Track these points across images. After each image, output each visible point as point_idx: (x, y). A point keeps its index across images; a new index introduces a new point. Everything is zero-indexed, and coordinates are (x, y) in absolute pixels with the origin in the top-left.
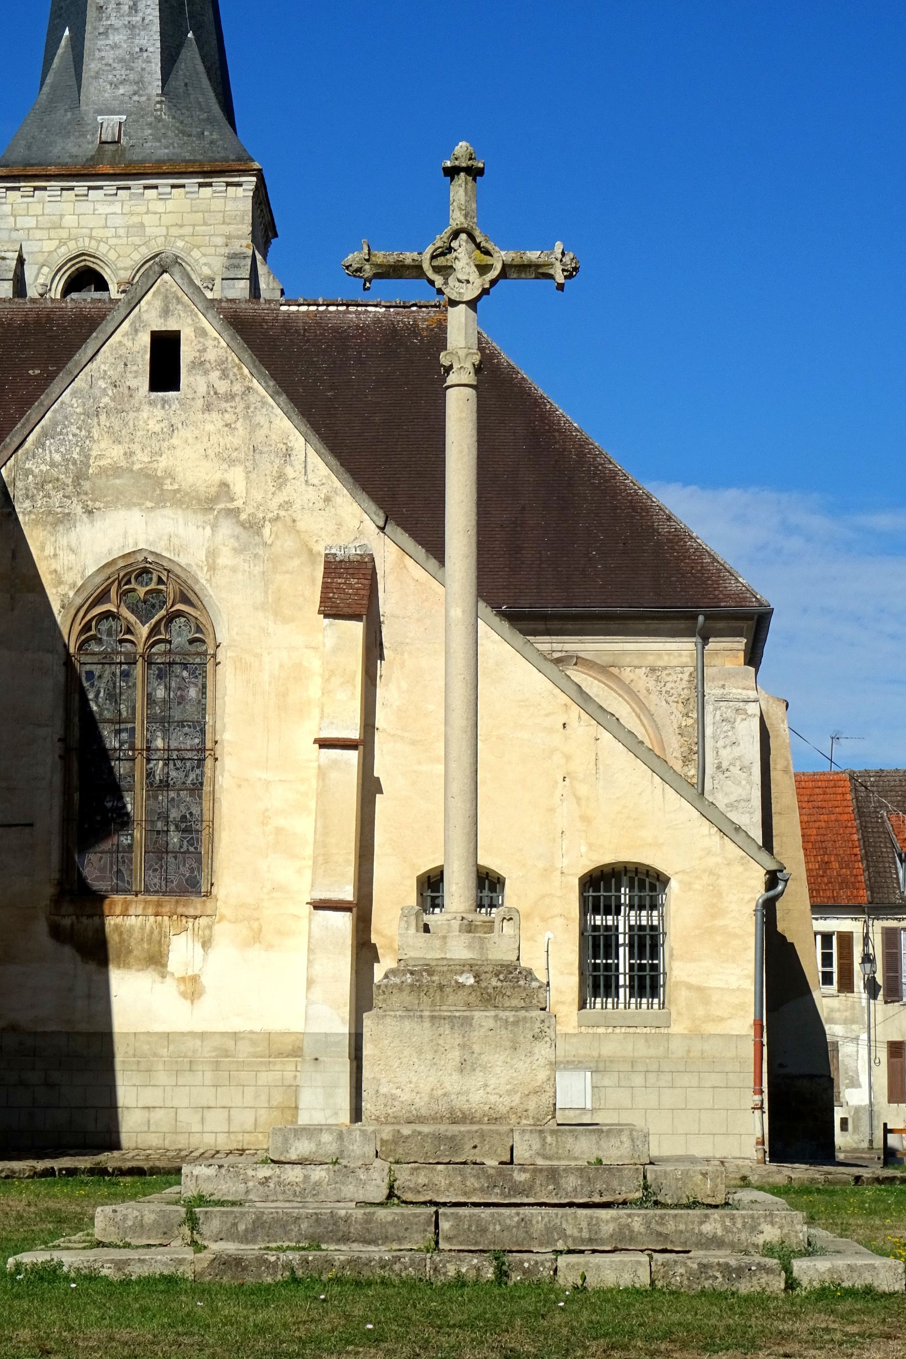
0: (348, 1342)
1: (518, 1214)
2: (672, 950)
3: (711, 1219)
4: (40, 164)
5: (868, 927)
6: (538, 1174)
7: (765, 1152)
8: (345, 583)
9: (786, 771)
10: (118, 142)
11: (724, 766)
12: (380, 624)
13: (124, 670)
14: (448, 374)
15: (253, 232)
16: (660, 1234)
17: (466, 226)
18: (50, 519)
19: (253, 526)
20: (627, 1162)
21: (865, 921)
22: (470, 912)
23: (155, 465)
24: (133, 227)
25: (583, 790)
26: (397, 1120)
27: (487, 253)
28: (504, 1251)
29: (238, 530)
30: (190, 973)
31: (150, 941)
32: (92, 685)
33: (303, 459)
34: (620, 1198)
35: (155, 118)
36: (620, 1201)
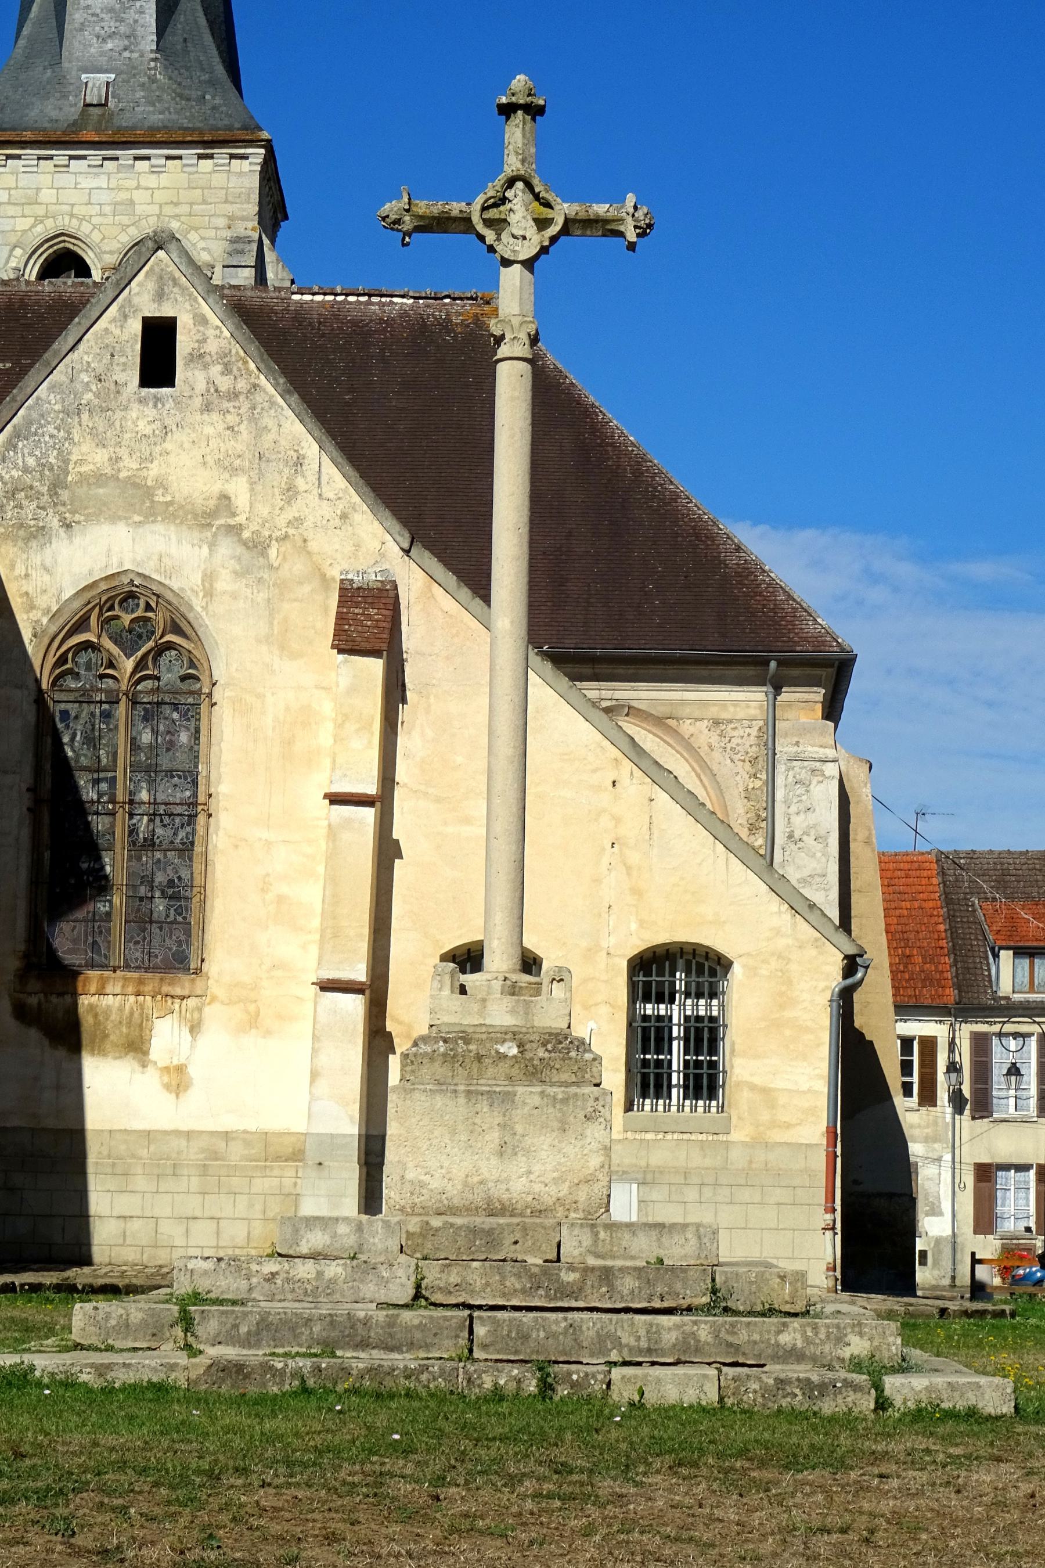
0: (371, 1452)
1: (566, 1319)
2: (733, 1044)
3: (790, 1329)
4: (15, 130)
5: (954, 1031)
6: (589, 1273)
7: (837, 1280)
8: (363, 614)
9: (868, 842)
10: (105, 105)
11: (797, 835)
12: (402, 662)
13: (105, 710)
14: (499, 346)
15: (260, 214)
16: (730, 1345)
17: (523, 172)
18: (22, 533)
19: (257, 546)
20: (692, 1262)
21: (951, 1025)
22: (514, 971)
23: (145, 473)
24: (121, 203)
25: (634, 857)
26: (425, 1211)
27: (548, 205)
28: (549, 1361)
29: (240, 550)
30: (175, 1062)
31: (129, 1024)
32: (67, 727)
33: (317, 469)
34: (685, 1303)
35: (149, 78)
36: (685, 1307)
